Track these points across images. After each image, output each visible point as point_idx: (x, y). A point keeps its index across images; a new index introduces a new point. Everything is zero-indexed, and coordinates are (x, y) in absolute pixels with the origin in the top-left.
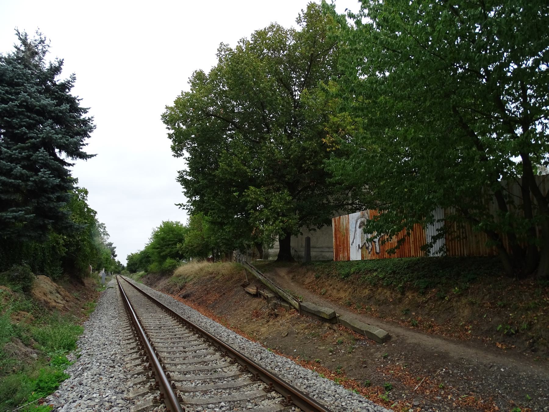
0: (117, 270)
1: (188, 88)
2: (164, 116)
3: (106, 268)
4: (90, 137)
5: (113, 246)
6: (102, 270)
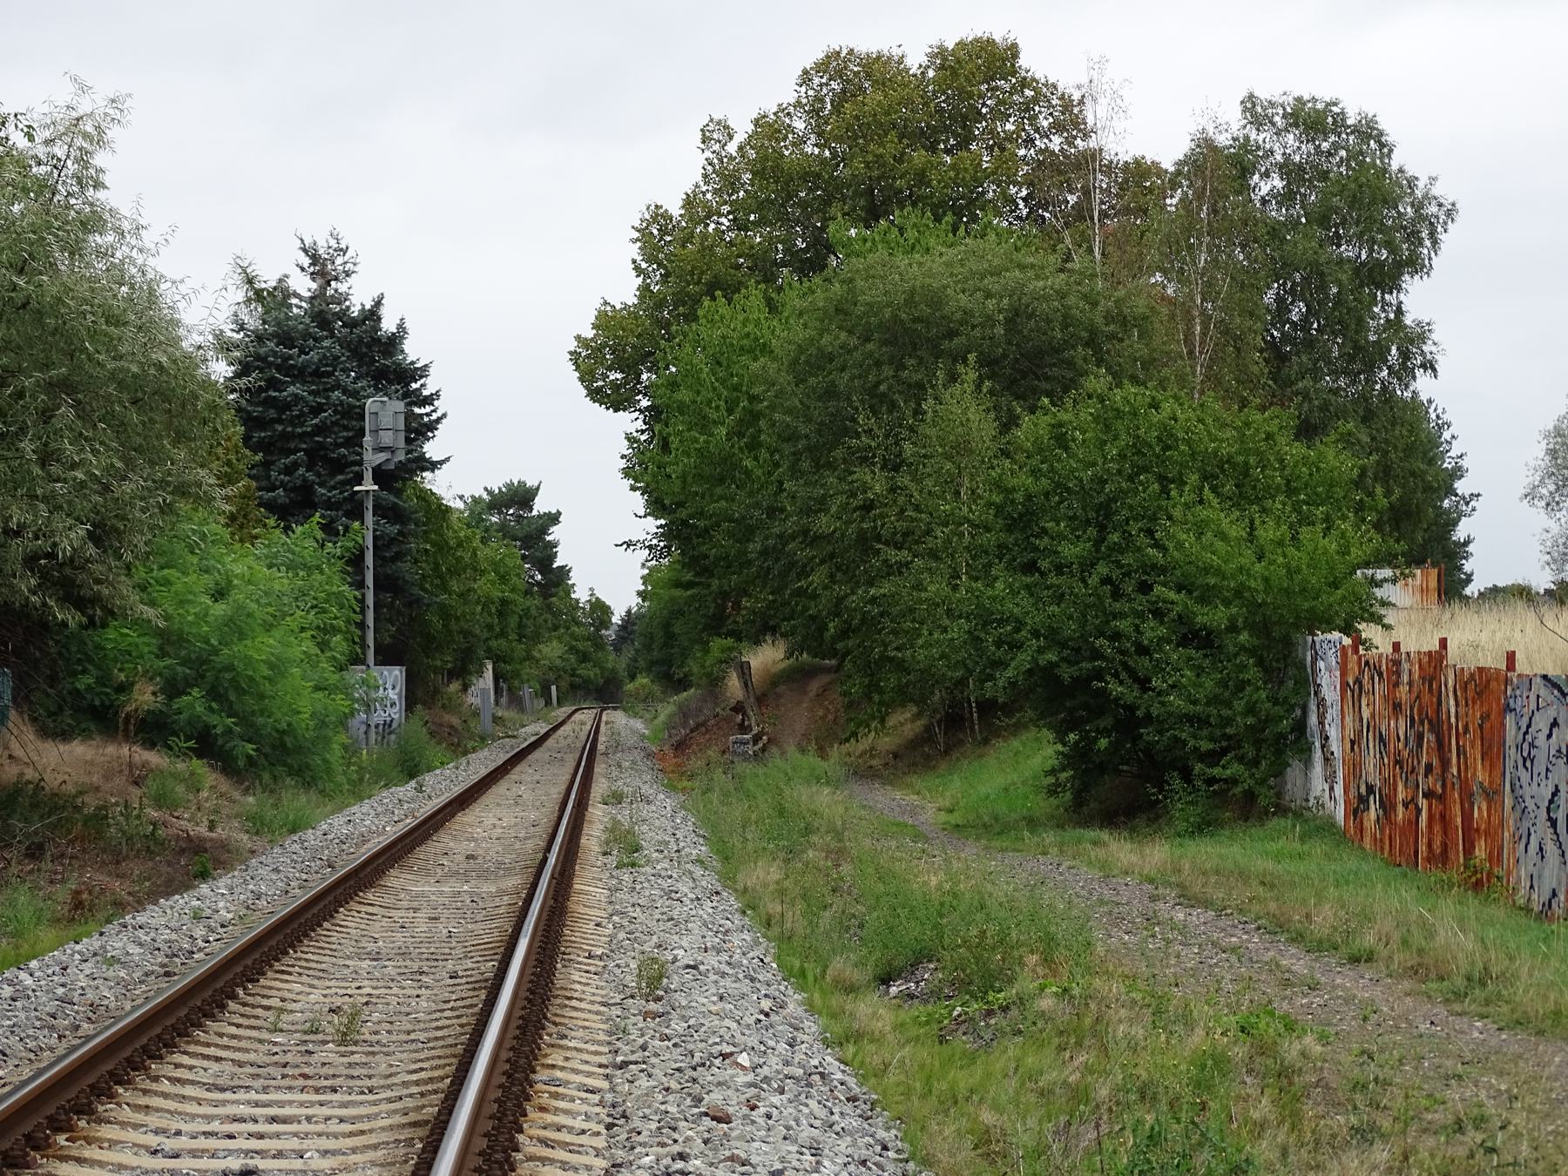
0: (588, 672)
1: (915, 59)
2: (1013, 51)
3: (498, 659)
4: (401, 327)
5: (541, 506)
6: (480, 673)
